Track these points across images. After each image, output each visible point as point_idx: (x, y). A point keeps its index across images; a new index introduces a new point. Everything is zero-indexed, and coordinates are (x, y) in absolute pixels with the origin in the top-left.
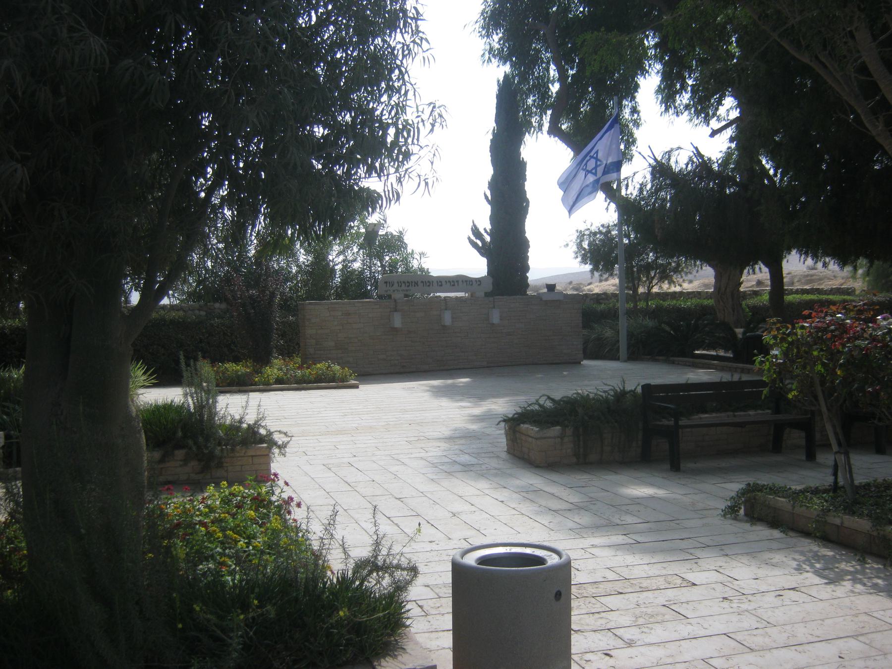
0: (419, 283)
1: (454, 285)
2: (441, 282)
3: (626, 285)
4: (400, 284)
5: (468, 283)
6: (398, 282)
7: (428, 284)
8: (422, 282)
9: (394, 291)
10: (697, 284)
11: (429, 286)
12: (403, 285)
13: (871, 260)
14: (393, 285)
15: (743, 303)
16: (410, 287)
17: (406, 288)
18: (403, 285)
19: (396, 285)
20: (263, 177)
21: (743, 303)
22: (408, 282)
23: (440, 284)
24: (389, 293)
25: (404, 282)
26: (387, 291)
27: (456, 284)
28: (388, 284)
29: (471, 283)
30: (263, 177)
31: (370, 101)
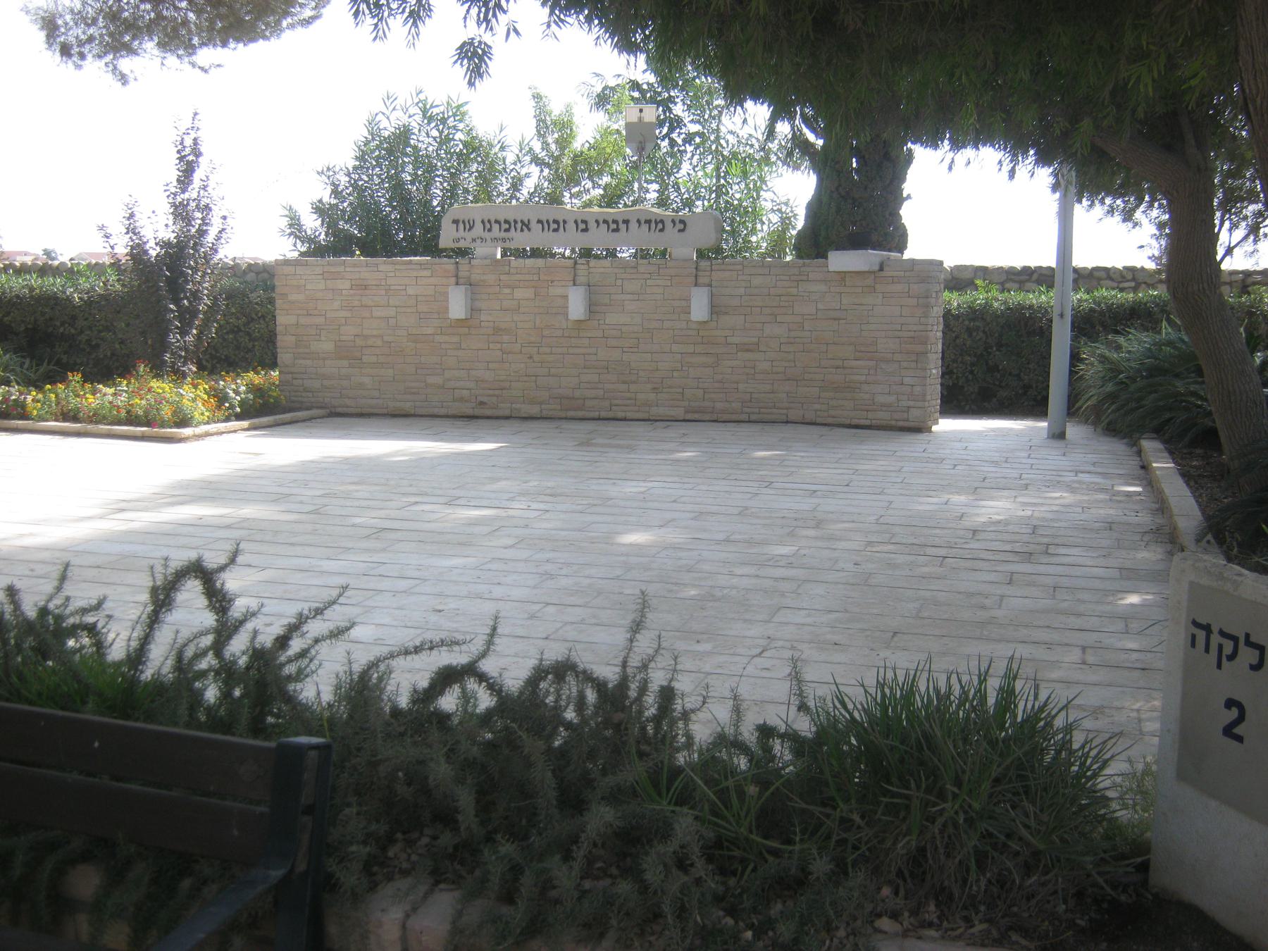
0: (534, 225)
1: (617, 230)
2: (584, 222)
3: (528, 249)
4: (488, 226)
5: (653, 225)
6: (483, 222)
7: (582, 226)
8: (539, 221)
9: (474, 240)
10: (589, 698)
11: (555, 230)
12: (495, 227)
13: (396, 712)
14: (471, 228)
15: (909, 145)
16: (512, 233)
17: (503, 234)
18: (495, 227)
19: (479, 226)
20: (854, 160)
21: (909, 145)
22: (506, 222)
23: (582, 226)
24: (462, 244)
25: (497, 222)
26: (458, 240)
27: (622, 227)
28: (461, 226)
29: (660, 226)
30: (854, 160)
31: (360, 177)
